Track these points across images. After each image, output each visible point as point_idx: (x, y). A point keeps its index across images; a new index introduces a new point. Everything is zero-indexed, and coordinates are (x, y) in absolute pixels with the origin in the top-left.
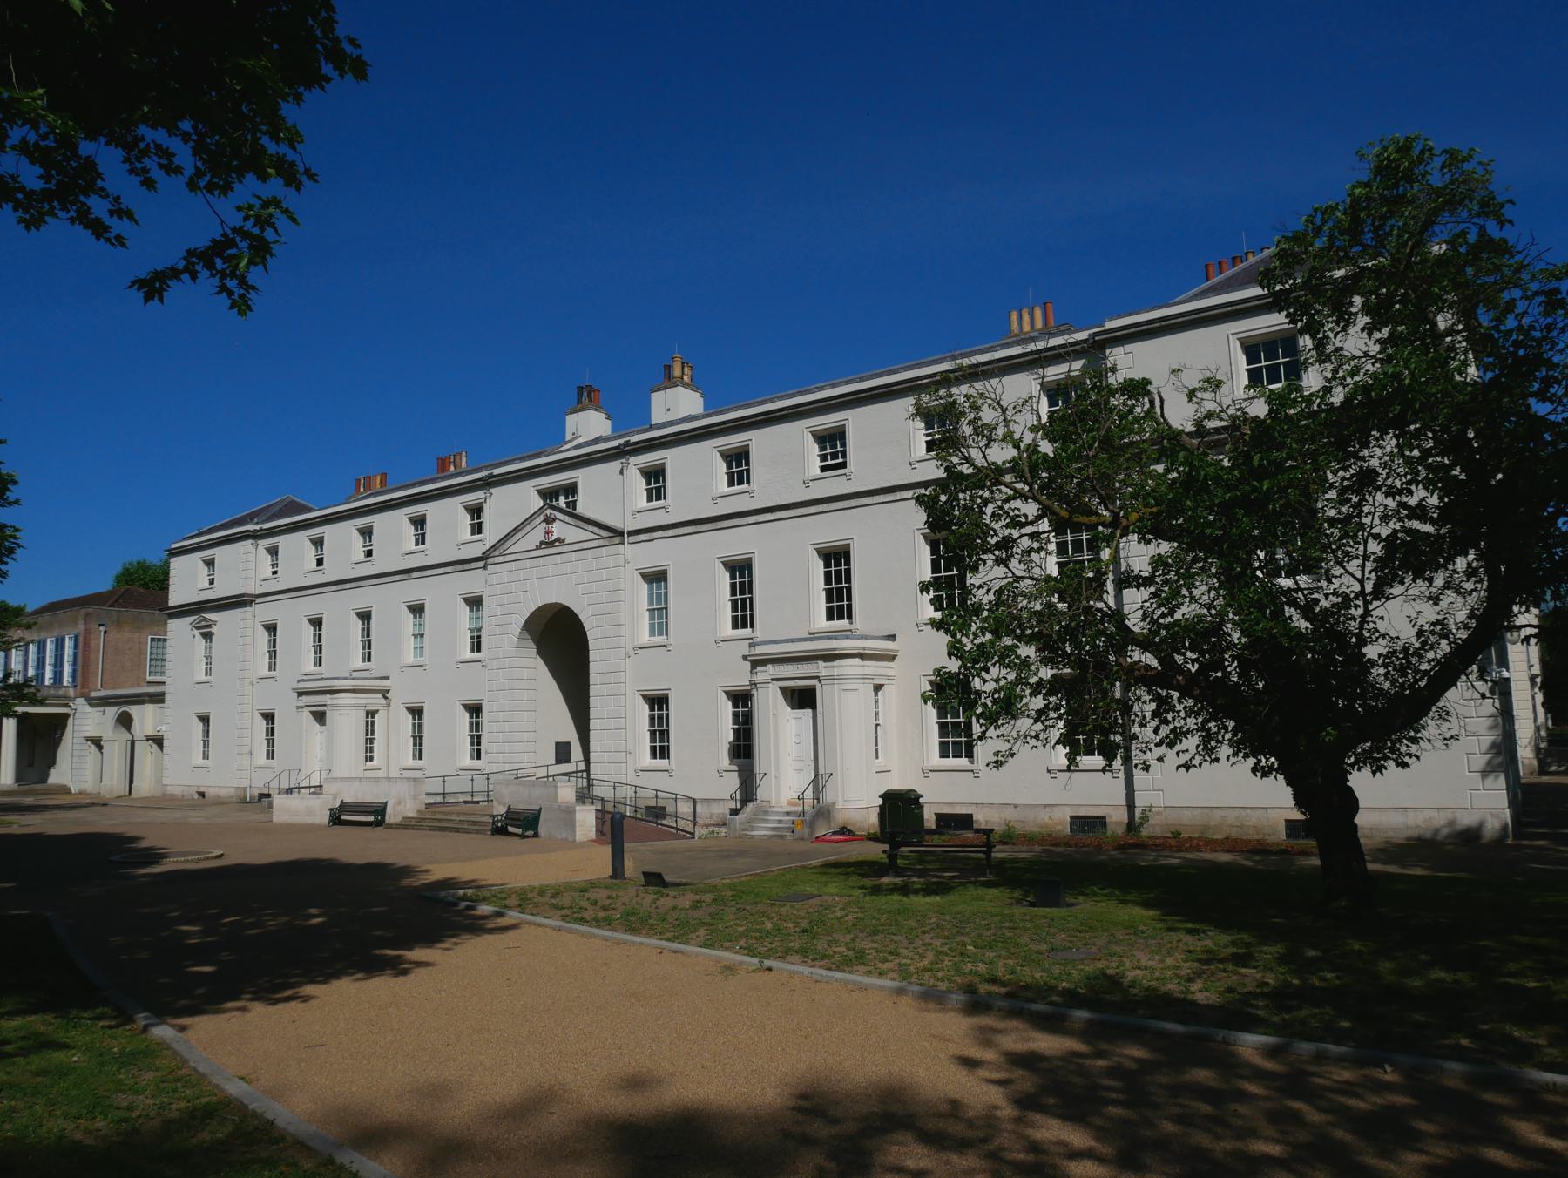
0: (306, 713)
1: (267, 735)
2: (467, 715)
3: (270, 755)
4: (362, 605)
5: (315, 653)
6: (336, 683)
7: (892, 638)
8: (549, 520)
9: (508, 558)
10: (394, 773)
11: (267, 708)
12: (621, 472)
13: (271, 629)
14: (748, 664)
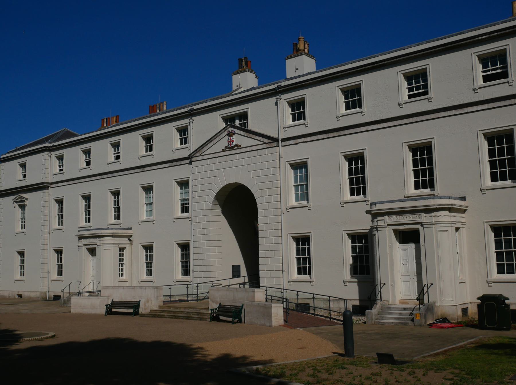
0: (84, 250)
1: (58, 262)
2: (145, 251)
3: (60, 273)
4: (85, 192)
5: (86, 215)
6: (102, 231)
7: (463, 199)
8: (230, 134)
9: (205, 157)
10: (135, 284)
11: (58, 246)
12: (276, 104)
13: (60, 202)
14: (78, 238)
